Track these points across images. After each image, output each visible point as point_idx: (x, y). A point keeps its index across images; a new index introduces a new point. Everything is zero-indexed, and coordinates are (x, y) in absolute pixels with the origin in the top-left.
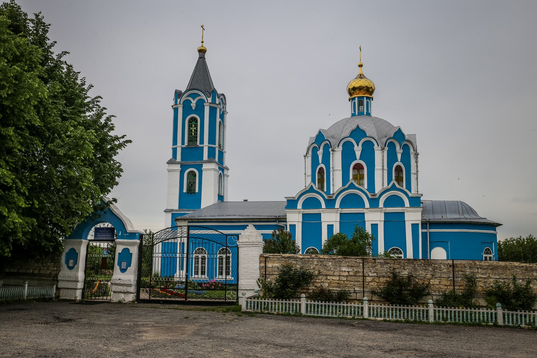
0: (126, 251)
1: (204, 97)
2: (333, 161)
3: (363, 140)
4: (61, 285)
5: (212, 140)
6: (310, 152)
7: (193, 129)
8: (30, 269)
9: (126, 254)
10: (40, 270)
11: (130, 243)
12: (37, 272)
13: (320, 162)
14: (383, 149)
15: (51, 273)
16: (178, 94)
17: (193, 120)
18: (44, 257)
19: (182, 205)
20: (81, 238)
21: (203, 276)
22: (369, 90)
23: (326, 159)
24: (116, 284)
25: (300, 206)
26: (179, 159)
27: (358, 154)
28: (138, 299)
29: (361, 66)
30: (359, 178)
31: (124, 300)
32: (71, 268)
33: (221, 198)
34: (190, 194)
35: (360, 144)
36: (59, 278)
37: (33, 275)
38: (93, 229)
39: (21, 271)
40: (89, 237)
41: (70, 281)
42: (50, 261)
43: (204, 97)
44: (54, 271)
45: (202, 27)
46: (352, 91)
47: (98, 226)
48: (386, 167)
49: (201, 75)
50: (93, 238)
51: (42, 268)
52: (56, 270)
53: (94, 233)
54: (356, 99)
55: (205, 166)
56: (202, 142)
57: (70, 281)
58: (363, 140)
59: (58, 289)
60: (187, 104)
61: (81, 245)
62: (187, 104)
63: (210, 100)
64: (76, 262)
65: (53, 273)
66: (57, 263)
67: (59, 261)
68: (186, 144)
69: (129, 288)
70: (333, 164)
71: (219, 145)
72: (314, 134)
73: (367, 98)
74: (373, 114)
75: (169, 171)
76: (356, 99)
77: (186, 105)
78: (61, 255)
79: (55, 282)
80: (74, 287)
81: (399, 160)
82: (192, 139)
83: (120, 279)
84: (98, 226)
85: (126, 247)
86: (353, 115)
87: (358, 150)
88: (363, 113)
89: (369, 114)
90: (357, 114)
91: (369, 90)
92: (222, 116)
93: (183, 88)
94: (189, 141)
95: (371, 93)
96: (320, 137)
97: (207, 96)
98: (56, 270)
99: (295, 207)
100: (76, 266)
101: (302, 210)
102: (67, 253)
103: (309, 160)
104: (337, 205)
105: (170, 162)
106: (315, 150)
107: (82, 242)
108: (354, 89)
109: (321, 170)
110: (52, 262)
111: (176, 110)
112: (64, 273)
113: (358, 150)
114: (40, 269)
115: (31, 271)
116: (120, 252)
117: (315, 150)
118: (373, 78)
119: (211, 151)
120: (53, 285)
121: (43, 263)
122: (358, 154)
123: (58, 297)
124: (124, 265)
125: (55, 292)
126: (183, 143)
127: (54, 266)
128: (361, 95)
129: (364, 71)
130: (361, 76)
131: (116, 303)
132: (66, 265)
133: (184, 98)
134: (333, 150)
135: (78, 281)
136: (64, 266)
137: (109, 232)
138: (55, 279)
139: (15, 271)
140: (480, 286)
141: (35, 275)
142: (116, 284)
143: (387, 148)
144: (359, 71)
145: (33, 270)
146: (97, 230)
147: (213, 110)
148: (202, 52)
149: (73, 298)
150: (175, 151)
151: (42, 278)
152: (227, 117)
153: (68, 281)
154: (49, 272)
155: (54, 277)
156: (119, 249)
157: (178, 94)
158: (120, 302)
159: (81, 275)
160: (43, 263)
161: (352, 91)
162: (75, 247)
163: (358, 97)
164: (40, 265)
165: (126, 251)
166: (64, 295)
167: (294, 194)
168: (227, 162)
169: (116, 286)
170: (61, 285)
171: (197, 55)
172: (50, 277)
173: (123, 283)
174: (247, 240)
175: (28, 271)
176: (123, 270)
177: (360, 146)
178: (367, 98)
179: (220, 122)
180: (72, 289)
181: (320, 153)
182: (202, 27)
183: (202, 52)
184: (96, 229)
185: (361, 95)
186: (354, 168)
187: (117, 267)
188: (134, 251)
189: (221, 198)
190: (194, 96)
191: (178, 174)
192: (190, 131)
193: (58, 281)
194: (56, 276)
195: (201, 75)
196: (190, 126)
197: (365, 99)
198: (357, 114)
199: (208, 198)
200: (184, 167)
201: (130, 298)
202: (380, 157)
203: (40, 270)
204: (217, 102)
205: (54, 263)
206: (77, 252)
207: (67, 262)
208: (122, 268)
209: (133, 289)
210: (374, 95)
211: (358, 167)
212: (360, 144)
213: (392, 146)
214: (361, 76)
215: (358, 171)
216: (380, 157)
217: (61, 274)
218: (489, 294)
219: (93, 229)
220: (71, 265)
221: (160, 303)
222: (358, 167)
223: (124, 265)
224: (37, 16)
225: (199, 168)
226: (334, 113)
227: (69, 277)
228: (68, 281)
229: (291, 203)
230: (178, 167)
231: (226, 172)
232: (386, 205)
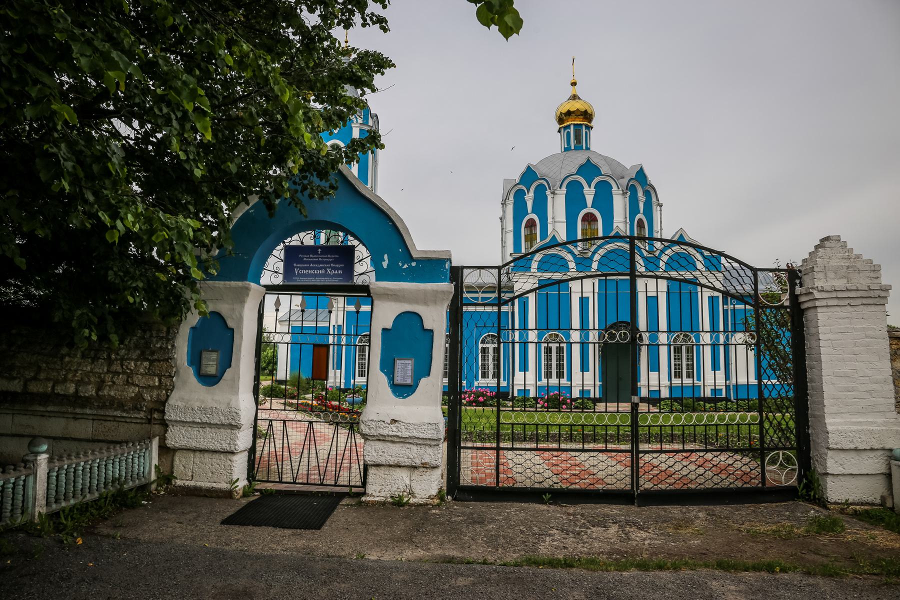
0: (409, 321)
2: (553, 208)
3: (596, 180)
4: (176, 437)
6: (511, 198)
8: (65, 380)
10: (100, 386)
11: (425, 292)
12: (90, 391)
13: (530, 210)
14: (624, 194)
15: (139, 397)
18: (114, 338)
20: (244, 278)
21: (487, 380)
22: (587, 116)
23: (541, 206)
24: (382, 439)
27: (589, 199)
28: (454, 488)
29: (574, 84)
31: (412, 493)
32: (210, 380)
35: (593, 185)
36: (170, 415)
37: (77, 400)
38: (279, 252)
39: (34, 388)
40: (267, 278)
41: (210, 425)
42: (135, 354)
44: (150, 388)
47: (294, 241)
50: (278, 280)
51: (108, 378)
52: (159, 387)
53: (281, 265)
54: (572, 127)
57: (210, 425)
58: (596, 180)
59: (166, 451)
61: (242, 302)
64: (227, 362)
65: (147, 397)
67: (167, 358)
69: (430, 451)
70: (553, 213)
72: (523, 169)
74: (592, 149)
76: (572, 127)
78: (175, 334)
79: (157, 428)
80: (225, 446)
81: (642, 211)
83: (394, 421)
84: (294, 241)
86: (567, 149)
87: (589, 194)
88: (581, 148)
89: (588, 149)
90: (573, 148)
95: (590, 120)
96: (529, 175)
98: (159, 387)
100: (228, 373)
101: (539, 274)
102: (193, 328)
106: (519, 197)
107: (248, 289)
108: (569, 113)
109: (531, 224)
110: (142, 357)
112: (188, 396)
113: (589, 194)
114: (103, 381)
115: (72, 388)
116: (389, 325)
118: (590, 99)
120: (150, 438)
121: (110, 362)
122: (589, 199)
123: (166, 478)
124: (404, 369)
125: (155, 461)
127: (150, 373)
128: (576, 122)
129: (578, 90)
130: (574, 97)
131: (384, 503)
132: (191, 371)
134: (553, 193)
135: (237, 427)
136: (188, 374)
137: (336, 261)
138: (156, 417)
139: (16, 386)
141: (85, 402)
142: (382, 439)
144: (571, 90)
145: (79, 383)
146: (293, 255)
149: (224, 486)
151: (110, 413)
153: (203, 425)
154: (132, 392)
155: (151, 411)
158: (398, 503)
160: (110, 362)
162: (224, 308)
163: (575, 125)
164: (101, 368)
165: (409, 321)
166: (191, 473)
169: (379, 445)
170: (176, 437)
172: (136, 409)
173: (406, 434)
174: (840, 284)
175: (59, 389)
176: (403, 390)
177: (593, 190)
180: (215, 452)
181: (529, 198)
184: (289, 250)
185: (576, 122)
186: (583, 220)
188: (436, 319)
193: (165, 425)
194: (160, 405)
197: (584, 127)
198: (573, 148)
201: (428, 486)
203: (100, 386)
205: (152, 362)
206: (230, 324)
207: (196, 361)
208: (398, 380)
209: (439, 455)
210: (592, 124)
212: (593, 185)
213: (632, 189)
214: (574, 97)
215: (589, 224)
217: (175, 400)
219: (279, 252)
220: (211, 368)
221: (542, 502)
222: (531, 224)
223: (404, 369)
227: (203, 410)
228: (203, 425)
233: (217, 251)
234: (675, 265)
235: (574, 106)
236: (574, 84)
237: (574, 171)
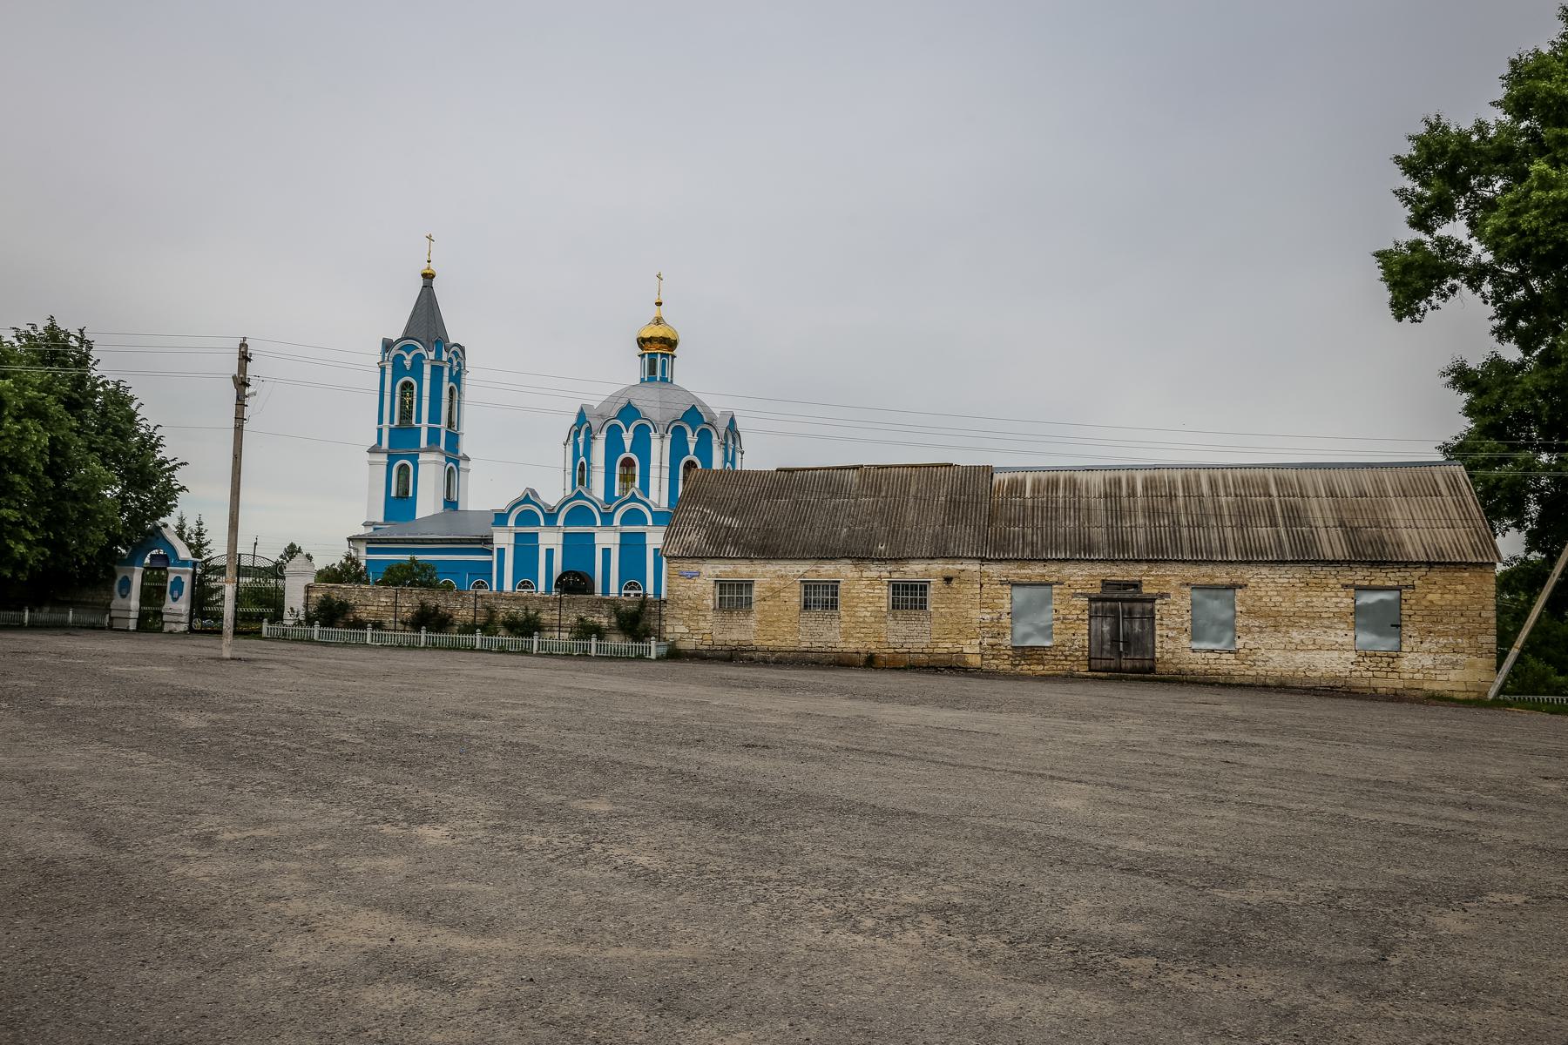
1: (423, 351)
3: (634, 424)
4: (114, 614)
5: (435, 416)
7: (407, 400)
9: (178, 583)
16: (387, 345)
17: (407, 385)
19: (389, 515)
22: (670, 344)
25: (511, 522)
26: (385, 445)
27: (628, 444)
28: (191, 630)
29: (659, 304)
30: (627, 478)
32: (124, 596)
33: (451, 504)
34: (400, 501)
35: (631, 429)
37: (86, 603)
43: (423, 351)
45: (429, 237)
46: (643, 342)
47: (155, 552)
48: (666, 463)
49: (426, 318)
55: (422, 457)
56: (419, 420)
58: (634, 424)
59: (111, 618)
60: (398, 360)
62: (398, 360)
63: (432, 355)
66: (110, 590)
68: (396, 422)
71: (450, 424)
73: (663, 355)
75: (371, 463)
77: (398, 362)
82: (406, 415)
85: (1119, 573)
86: (642, 380)
87: (628, 438)
91: (670, 344)
92: (457, 378)
93: (396, 333)
94: (401, 418)
97: (429, 349)
99: (505, 524)
103: (570, 449)
104: (560, 521)
105: (373, 450)
108: (650, 340)
111: (383, 369)
112: (117, 602)
113: (628, 438)
117: (577, 433)
118: (676, 324)
119: (434, 435)
122: (628, 444)
124: (176, 594)
126: (392, 422)
128: (658, 350)
129: (664, 312)
130: (658, 321)
133: (394, 352)
140: (501, 616)
143: (670, 435)
144: (655, 312)
147: (437, 372)
148: (428, 277)
150: (380, 431)
152: (467, 379)
156: (171, 577)
157: (387, 345)
159: (134, 603)
161: (643, 342)
167: (502, 505)
168: (465, 447)
171: (420, 282)
178: (663, 355)
179: (451, 390)
182: (429, 237)
183: (428, 277)
185: (658, 350)
186: (622, 464)
187: (168, 596)
188: (186, 579)
189: (451, 504)
190: (408, 348)
191: (384, 468)
192: (402, 402)
195: (426, 318)
196: (403, 396)
199: (428, 503)
200: (392, 459)
201: (183, 628)
202: (660, 449)
204: (445, 358)
209: (185, 619)
211: (628, 463)
212: (631, 429)
214: (658, 321)
216: (660, 449)
218: (505, 624)
222: (628, 463)
223: (176, 594)
224: (81, 331)
225: (414, 459)
226: (615, 375)
229: (500, 518)
230: (384, 458)
231: (462, 464)
232: (624, 521)
233: (1532, 168)
234: (158, 564)
235: (658, 332)
236: (659, 304)
237: (614, 413)
